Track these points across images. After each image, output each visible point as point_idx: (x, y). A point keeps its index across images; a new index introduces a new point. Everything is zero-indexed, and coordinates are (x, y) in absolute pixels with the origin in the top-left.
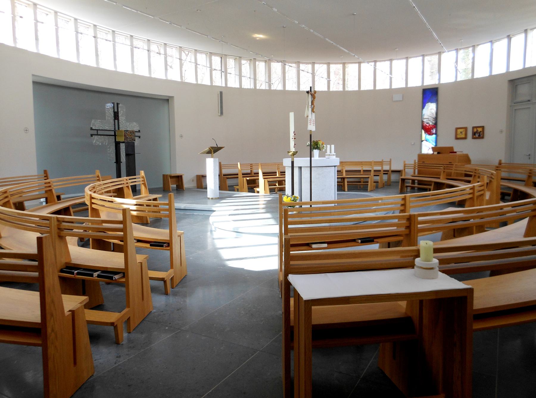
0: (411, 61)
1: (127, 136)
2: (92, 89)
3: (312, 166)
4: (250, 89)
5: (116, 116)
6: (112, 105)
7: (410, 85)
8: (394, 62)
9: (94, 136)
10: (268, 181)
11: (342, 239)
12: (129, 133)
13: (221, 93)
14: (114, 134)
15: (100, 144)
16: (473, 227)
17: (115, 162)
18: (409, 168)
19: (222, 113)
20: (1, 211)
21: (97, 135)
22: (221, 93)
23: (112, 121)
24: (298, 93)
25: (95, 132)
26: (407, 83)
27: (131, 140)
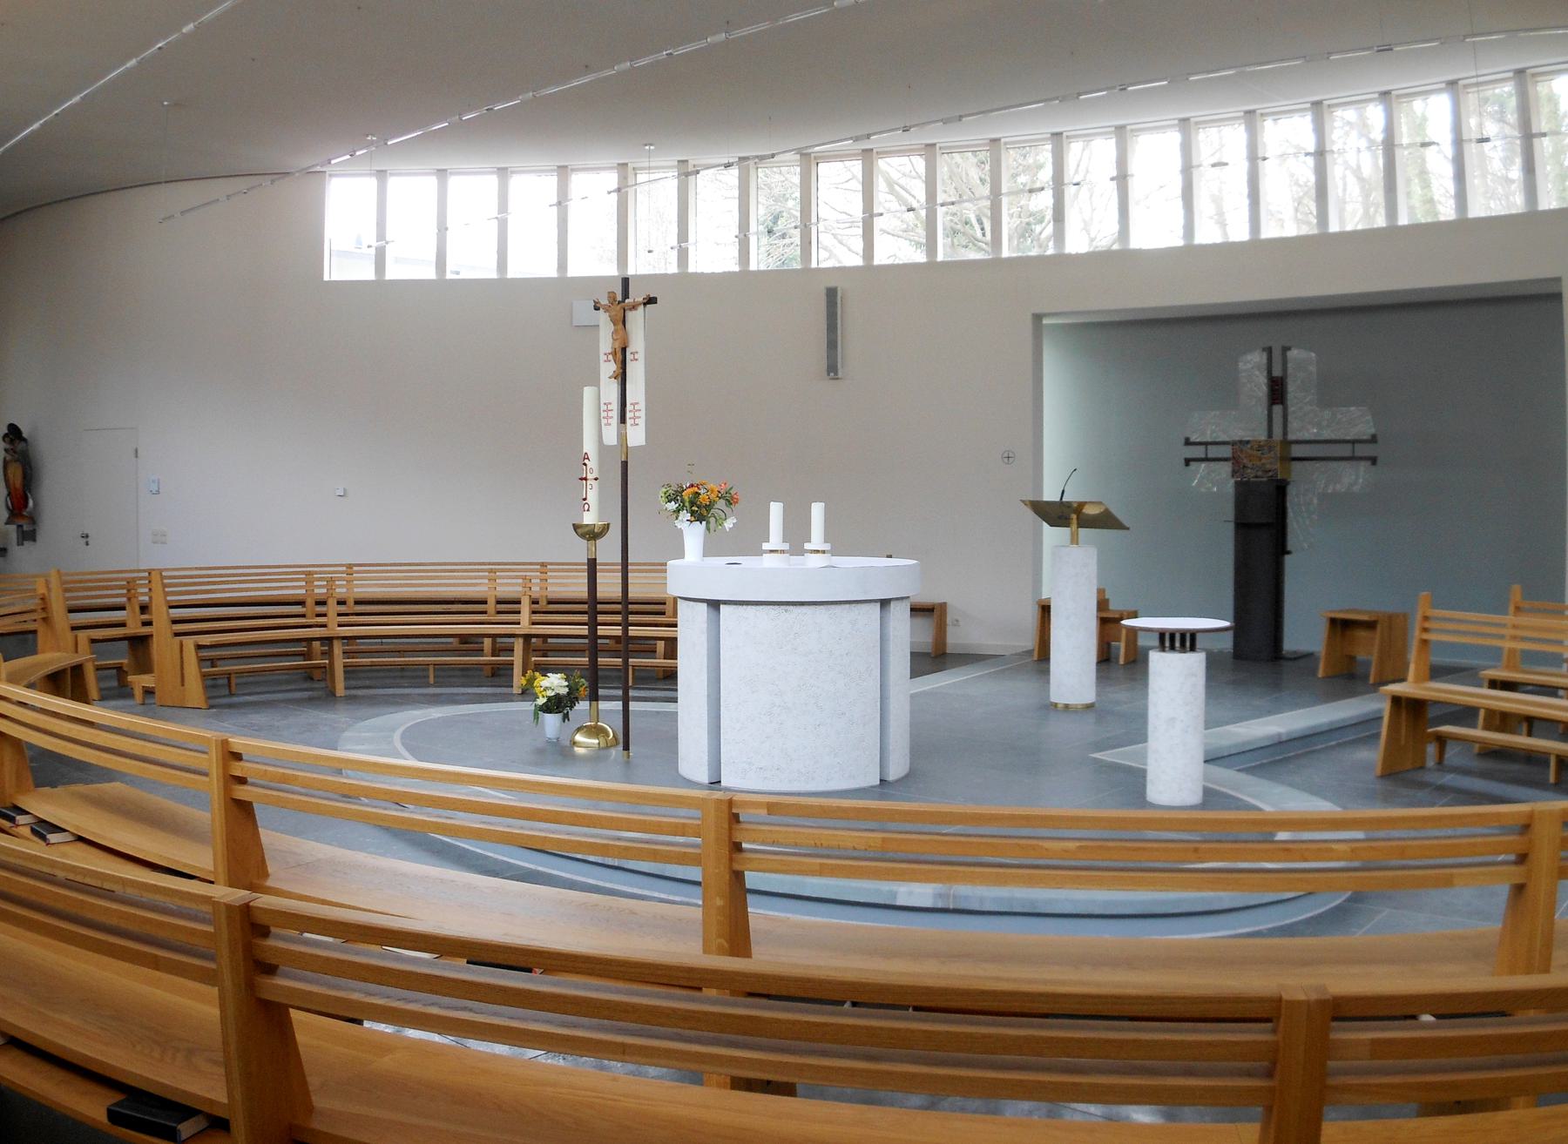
0: (517, 183)
1: (1245, 461)
2: (1388, 301)
3: (629, 561)
4: (665, 276)
5: (1277, 391)
6: (1265, 356)
7: (513, 272)
8: (454, 182)
9: (1193, 465)
10: (199, 647)
11: (622, 812)
12: (1252, 448)
13: (831, 294)
14: (1356, 454)
15: (1215, 489)
16: (1327, 677)
17: (1289, 553)
18: (401, 565)
19: (832, 368)
20: (5, 889)
21: (1206, 459)
22: (831, 294)
23: (1261, 411)
24: (563, 287)
25: (1198, 452)
26: (562, 264)
27: (1260, 473)
